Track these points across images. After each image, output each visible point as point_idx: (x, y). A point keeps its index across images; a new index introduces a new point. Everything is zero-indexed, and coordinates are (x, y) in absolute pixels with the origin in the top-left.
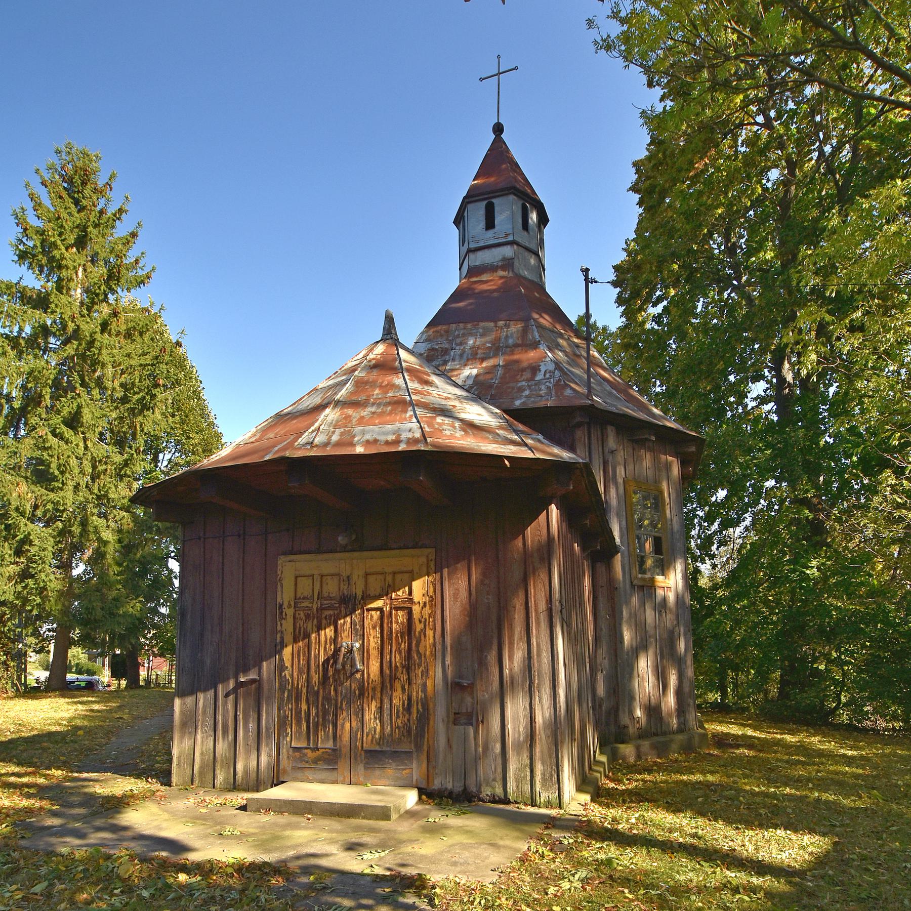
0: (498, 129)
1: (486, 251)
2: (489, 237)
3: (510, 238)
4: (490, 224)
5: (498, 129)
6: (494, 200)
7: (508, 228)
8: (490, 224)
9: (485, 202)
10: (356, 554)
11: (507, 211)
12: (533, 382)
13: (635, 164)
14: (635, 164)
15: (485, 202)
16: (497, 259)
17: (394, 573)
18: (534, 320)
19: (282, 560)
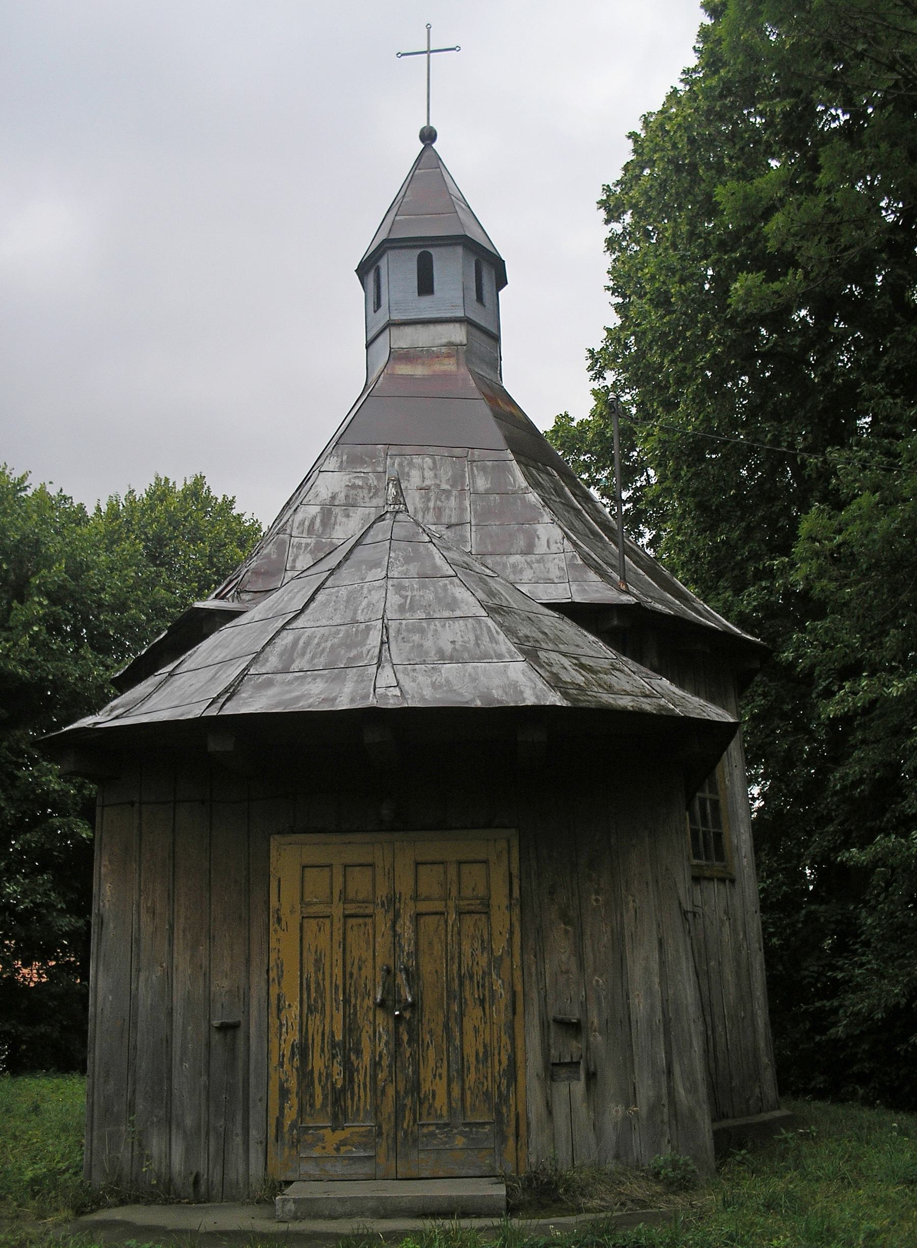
0: (428, 136)
1: (419, 327)
2: (426, 307)
3: (460, 314)
4: (426, 286)
5: (428, 136)
6: (431, 250)
7: (456, 295)
8: (426, 286)
9: (419, 251)
10: (397, 835)
11: (451, 272)
12: (533, 557)
13: (199, 481)
14: (199, 481)
15: (419, 251)
16: (438, 342)
17: (460, 863)
18: (648, 475)
19: (209, 750)
